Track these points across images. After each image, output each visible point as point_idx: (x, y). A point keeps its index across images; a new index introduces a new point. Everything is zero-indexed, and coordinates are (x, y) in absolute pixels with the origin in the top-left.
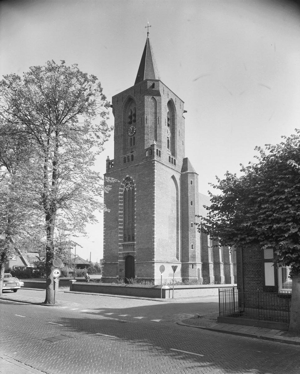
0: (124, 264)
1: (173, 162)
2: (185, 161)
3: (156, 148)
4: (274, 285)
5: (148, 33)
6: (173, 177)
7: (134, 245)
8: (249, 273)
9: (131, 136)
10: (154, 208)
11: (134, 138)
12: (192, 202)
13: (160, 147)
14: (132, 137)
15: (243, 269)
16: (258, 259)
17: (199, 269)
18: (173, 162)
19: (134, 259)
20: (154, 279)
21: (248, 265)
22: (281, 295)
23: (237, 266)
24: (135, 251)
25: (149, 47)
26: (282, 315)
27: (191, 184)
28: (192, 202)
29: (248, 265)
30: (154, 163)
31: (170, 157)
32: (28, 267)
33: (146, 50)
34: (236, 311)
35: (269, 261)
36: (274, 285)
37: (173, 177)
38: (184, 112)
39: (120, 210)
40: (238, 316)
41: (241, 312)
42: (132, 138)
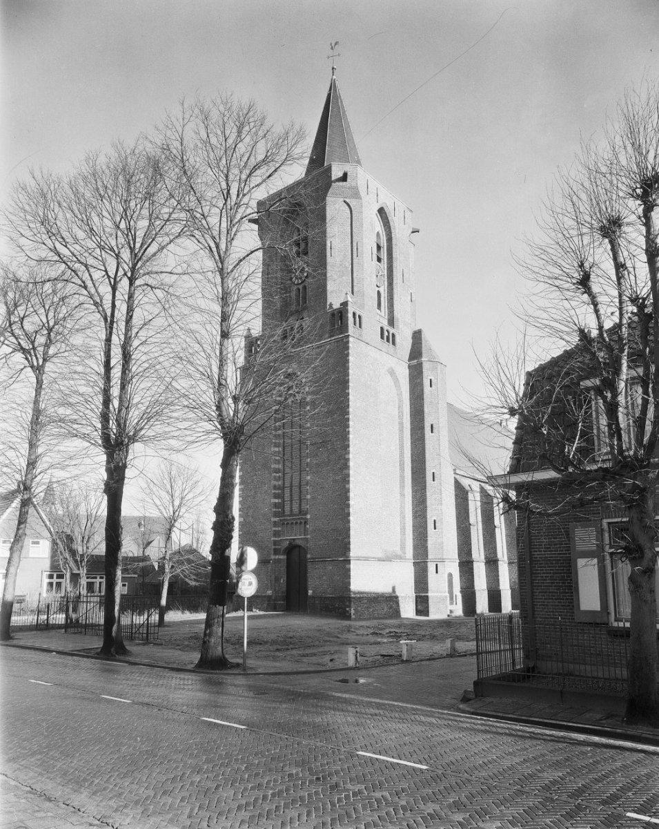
0: (284, 564)
1: (389, 338)
2: (417, 336)
3: (351, 309)
4: (599, 609)
5: (333, 68)
6: (392, 372)
7: (305, 522)
8: (543, 583)
9: (298, 284)
10: (348, 440)
11: (305, 288)
12: (432, 426)
13: (362, 306)
14: (301, 287)
15: (532, 574)
16: (562, 551)
17: (450, 575)
18: (389, 338)
19: (306, 553)
20: (427, 596)
21: (542, 564)
22: (616, 631)
23: (519, 567)
24: (309, 536)
25: (337, 98)
26: (578, 674)
27: (431, 386)
28: (432, 426)
29: (542, 564)
30: (348, 342)
31: (382, 329)
32: (74, 572)
33: (329, 103)
34: (518, 667)
35: (588, 554)
36: (599, 609)
37: (392, 372)
38: (413, 232)
39: (275, 446)
40: (524, 678)
41: (528, 670)
42: (299, 290)
